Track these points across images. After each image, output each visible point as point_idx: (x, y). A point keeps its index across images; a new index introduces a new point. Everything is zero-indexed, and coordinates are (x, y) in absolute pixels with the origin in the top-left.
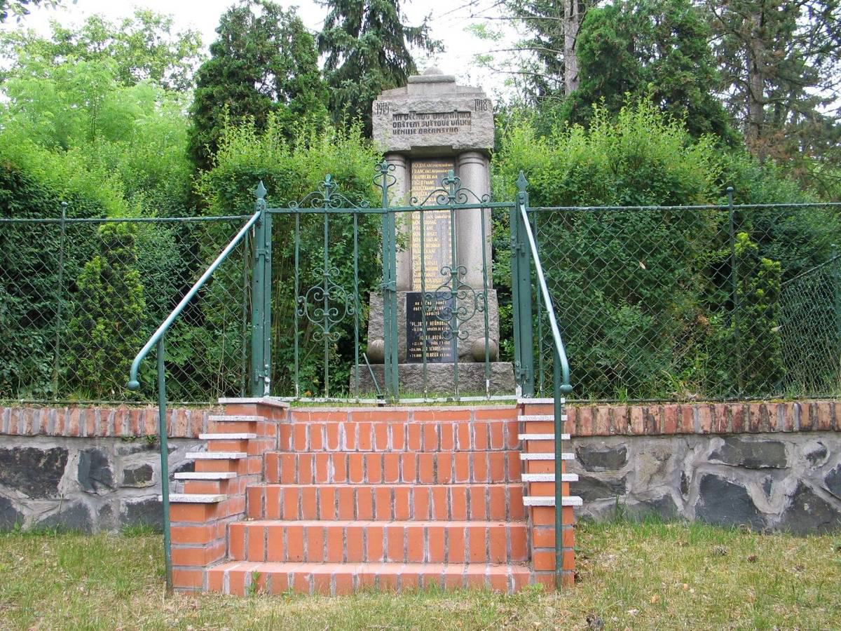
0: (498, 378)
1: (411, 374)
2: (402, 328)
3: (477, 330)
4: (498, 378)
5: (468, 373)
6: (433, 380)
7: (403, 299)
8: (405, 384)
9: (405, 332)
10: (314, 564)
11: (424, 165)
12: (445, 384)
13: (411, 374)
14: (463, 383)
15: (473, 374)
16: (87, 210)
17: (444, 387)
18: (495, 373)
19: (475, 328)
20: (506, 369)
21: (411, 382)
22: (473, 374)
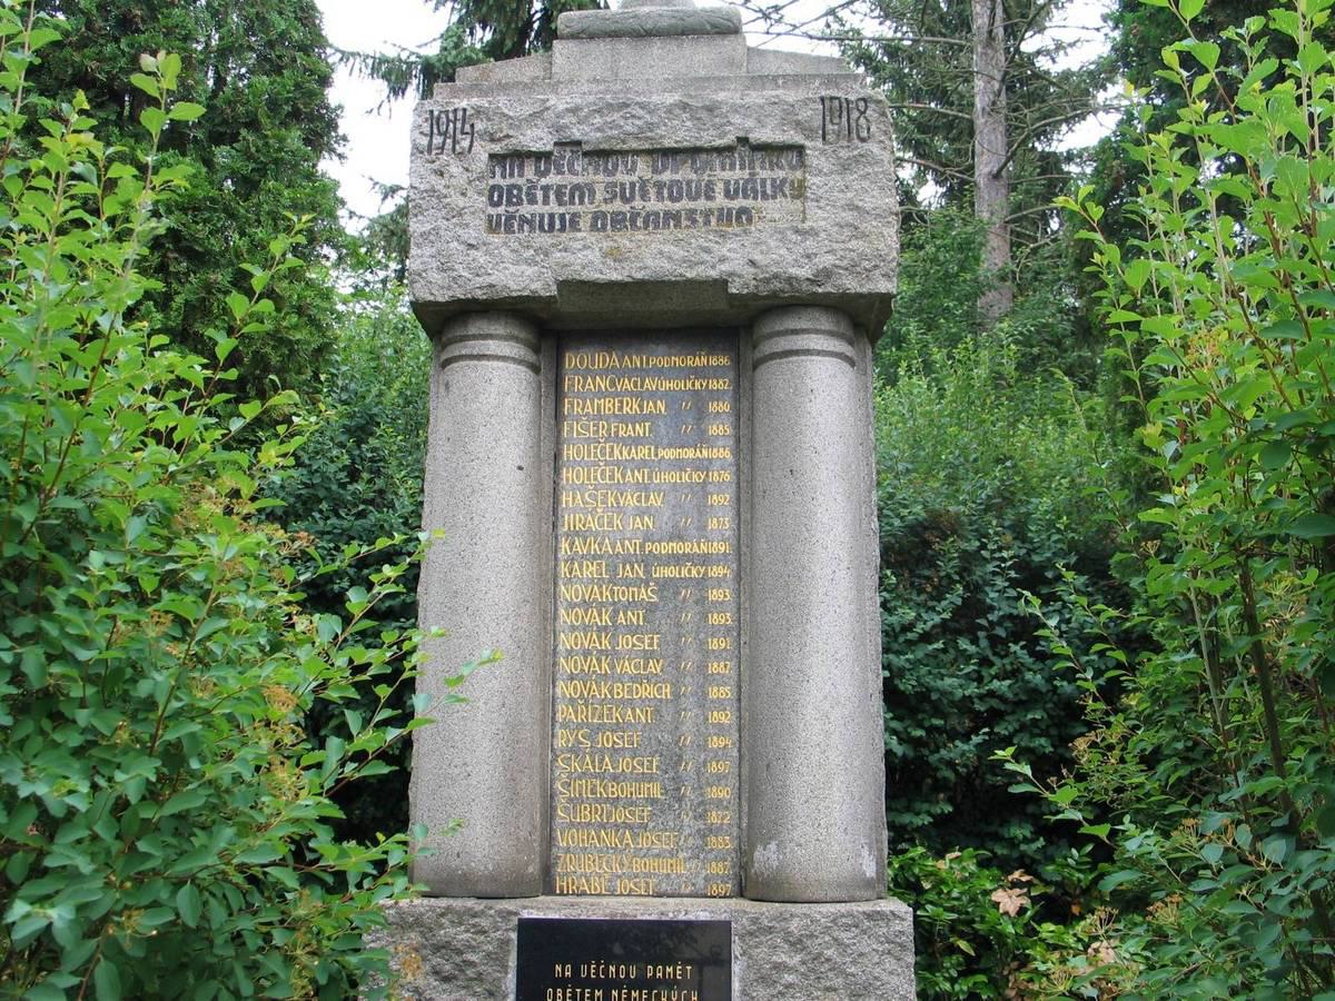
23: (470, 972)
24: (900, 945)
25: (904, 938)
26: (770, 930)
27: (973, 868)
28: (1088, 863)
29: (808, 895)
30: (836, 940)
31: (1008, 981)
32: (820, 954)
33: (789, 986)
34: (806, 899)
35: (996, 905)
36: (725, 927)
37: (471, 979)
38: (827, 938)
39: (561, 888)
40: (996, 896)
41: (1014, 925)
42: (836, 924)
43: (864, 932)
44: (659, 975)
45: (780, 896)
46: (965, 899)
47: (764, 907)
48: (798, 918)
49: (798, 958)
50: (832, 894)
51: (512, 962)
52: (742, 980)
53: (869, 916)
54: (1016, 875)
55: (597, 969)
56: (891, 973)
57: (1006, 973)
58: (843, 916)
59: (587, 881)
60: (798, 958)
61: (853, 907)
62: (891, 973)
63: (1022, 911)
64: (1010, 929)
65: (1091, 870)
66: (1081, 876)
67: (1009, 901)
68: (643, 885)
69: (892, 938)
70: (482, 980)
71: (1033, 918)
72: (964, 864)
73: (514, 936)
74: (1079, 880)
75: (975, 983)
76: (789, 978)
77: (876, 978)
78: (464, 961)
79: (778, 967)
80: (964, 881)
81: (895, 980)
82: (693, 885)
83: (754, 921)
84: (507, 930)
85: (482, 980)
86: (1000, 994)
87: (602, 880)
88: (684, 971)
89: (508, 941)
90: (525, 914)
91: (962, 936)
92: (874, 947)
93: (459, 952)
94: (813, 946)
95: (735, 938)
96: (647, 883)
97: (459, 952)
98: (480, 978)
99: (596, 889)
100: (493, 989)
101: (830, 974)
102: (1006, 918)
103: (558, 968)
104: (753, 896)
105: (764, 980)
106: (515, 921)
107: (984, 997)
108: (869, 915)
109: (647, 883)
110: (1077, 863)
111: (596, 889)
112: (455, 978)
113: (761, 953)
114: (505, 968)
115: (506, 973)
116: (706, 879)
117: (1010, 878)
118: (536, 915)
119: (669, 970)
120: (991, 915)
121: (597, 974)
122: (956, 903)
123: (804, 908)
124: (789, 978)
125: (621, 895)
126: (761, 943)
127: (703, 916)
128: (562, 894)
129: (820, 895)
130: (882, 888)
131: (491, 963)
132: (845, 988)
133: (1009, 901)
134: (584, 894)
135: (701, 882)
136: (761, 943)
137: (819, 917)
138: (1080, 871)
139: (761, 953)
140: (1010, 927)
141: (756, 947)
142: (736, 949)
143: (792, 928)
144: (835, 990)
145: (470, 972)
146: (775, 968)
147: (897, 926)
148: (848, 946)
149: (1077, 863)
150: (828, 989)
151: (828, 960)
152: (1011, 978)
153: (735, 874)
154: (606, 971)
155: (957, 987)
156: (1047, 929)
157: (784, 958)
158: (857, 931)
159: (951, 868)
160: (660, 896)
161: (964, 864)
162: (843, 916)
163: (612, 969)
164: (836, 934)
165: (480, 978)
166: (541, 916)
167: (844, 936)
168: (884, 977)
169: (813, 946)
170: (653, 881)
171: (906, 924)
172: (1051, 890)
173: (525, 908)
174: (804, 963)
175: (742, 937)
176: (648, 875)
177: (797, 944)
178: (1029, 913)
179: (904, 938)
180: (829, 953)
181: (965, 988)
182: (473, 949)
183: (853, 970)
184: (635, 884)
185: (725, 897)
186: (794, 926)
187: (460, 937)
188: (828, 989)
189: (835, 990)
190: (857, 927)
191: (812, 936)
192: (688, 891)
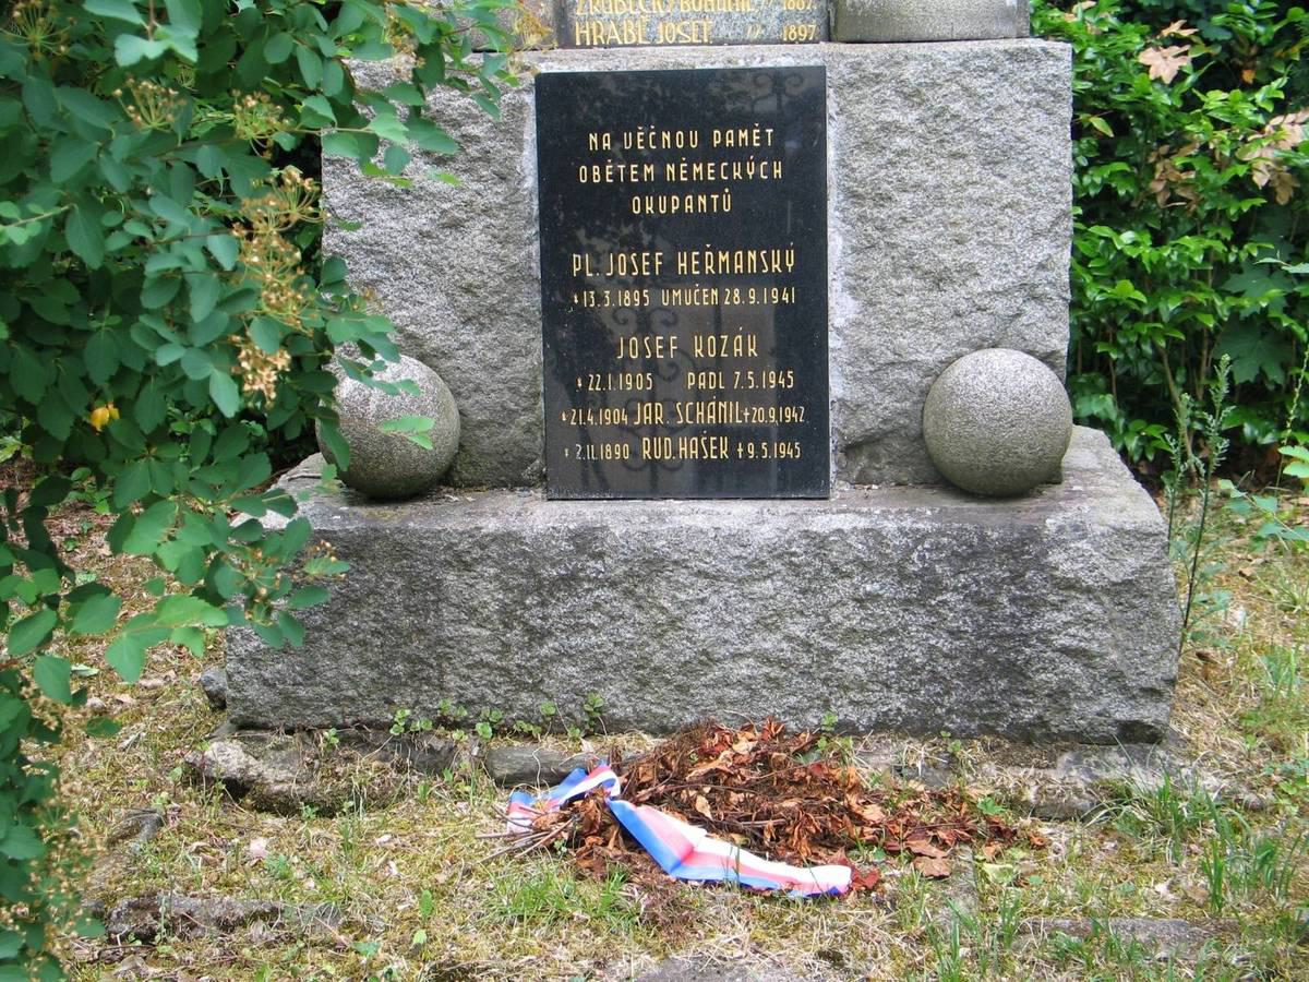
0: (1086, 621)
1: (570, 581)
2: (515, 276)
3: (954, 296)
4: (1086, 621)
5: (904, 577)
6: (700, 620)
7: (521, 107)
8: (537, 636)
9: (530, 299)
10: (733, 502)
11: (1001, 505)
12: (769, 643)
13: (570, 581)
14: (876, 636)
15: (934, 586)
16: (249, 8)
17: (764, 658)
18: (1071, 585)
19: (939, 280)
20: (1132, 562)
21: (576, 629)
22: (934, 586)
23: (473, 151)
24: (1053, 94)
25: (1059, 85)
26: (877, 79)
27: (1113, 21)
28: (1272, 10)
29: (928, 31)
30: (965, 89)
31: (1154, 171)
32: (944, 110)
33: (902, 152)
34: (925, 37)
35: (1146, 69)
36: (820, 71)
37: (475, 160)
38: (954, 88)
39: (583, 37)
40: (1143, 59)
41: (1170, 95)
42: (967, 68)
43: (1005, 78)
44: (730, 142)
45: (888, 35)
46: (1100, 64)
47: (868, 49)
48: (914, 62)
49: (914, 115)
50: (959, 30)
51: (530, 133)
52: (839, 146)
53: (1012, 56)
54: (1175, 28)
55: (645, 137)
56: (1040, 132)
57: (1152, 160)
58: (977, 57)
59: (618, 27)
60: (914, 115)
61: (990, 45)
62: (1040, 132)
63: (1180, 76)
64: (1166, 99)
65: (1275, 21)
66: (1261, 29)
67: (1164, 63)
68: (694, 29)
69: (1043, 84)
70: (488, 161)
71: (1194, 85)
72: (1103, 15)
73: (530, 99)
74: (1258, 35)
75: (1112, 174)
76: (902, 142)
77: (1019, 139)
78: (463, 136)
79: (885, 128)
80: (1103, 36)
81: (1044, 141)
82: (764, 27)
83: (856, 67)
84: (518, 92)
85: (488, 161)
86: (1141, 189)
87: (638, 23)
88: (763, 134)
89: (521, 107)
90: (543, 69)
91: (1095, 112)
92: (1018, 97)
93: (457, 125)
94: (935, 98)
95: (830, 91)
96: (700, 27)
97: (457, 125)
98: (485, 157)
99: (630, 37)
100: (504, 171)
101: (958, 136)
102: (1157, 86)
103: (593, 138)
104: (845, 39)
105: (867, 145)
106: (530, 78)
107: (1122, 192)
108: (1012, 55)
109: (700, 27)
110: (1258, 11)
111: (630, 37)
112: (452, 159)
113: (863, 111)
114: (518, 143)
115: (521, 150)
116: (781, 18)
117: (1165, 32)
118: (556, 68)
119: (743, 135)
120: (1138, 81)
121: (645, 143)
122: (1089, 67)
123: (923, 48)
124: (902, 142)
125: (666, 44)
126: (865, 96)
127: (785, 62)
128: (584, 46)
129: (944, 31)
130: (1023, 24)
131: (501, 136)
132: (977, 154)
133: (1164, 63)
134: (614, 44)
135: (773, 23)
136: (865, 96)
137: (943, 59)
138: (1259, 22)
139: (863, 111)
140: (1165, 96)
141: (858, 102)
142: (832, 107)
143: (907, 75)
144: (964, 156)
145: (473, 151)
146: (883, 129)
147: (1050, 68)
148: (982, 97)
149: (1258, 11)
150: (954, 156)
151: (955, 117)
152: (1159, 167)
153: (821, 10)
154: (657, 140)
155: (1087, 180)
156: (1215, 99)
157: (896, 116)
158: (995, 77)
159: (1084, 20)
160: (720, 43)
161: (1103, 15)
162: (977, 57)
163: (666, 136)
164: (966, 81)
165: (485, 157)
166: (565, 69)
167: (978, 84)
168: (1031, 137)
169: (935, 98)
170: (707, 25)
171: (1062, 65)
172: (1216, 50)
173: (542, 60)
174: (922, 121)
175: (839, 89)
176: (703, 15)
177: (912, 97)
178: (1190, 79)
179: (1059, 85)
180: (956, 107)
181: (1098, 180)
182: (475, 119)
183: (988, 129)
184: (684, 28)
185: (807, 41)
186: (910, 72)
187: (456, 104)
188: (954, 156)
189: (964, 156)
190: (994, 70)
191: (934, 85)
192: (756, 36)
